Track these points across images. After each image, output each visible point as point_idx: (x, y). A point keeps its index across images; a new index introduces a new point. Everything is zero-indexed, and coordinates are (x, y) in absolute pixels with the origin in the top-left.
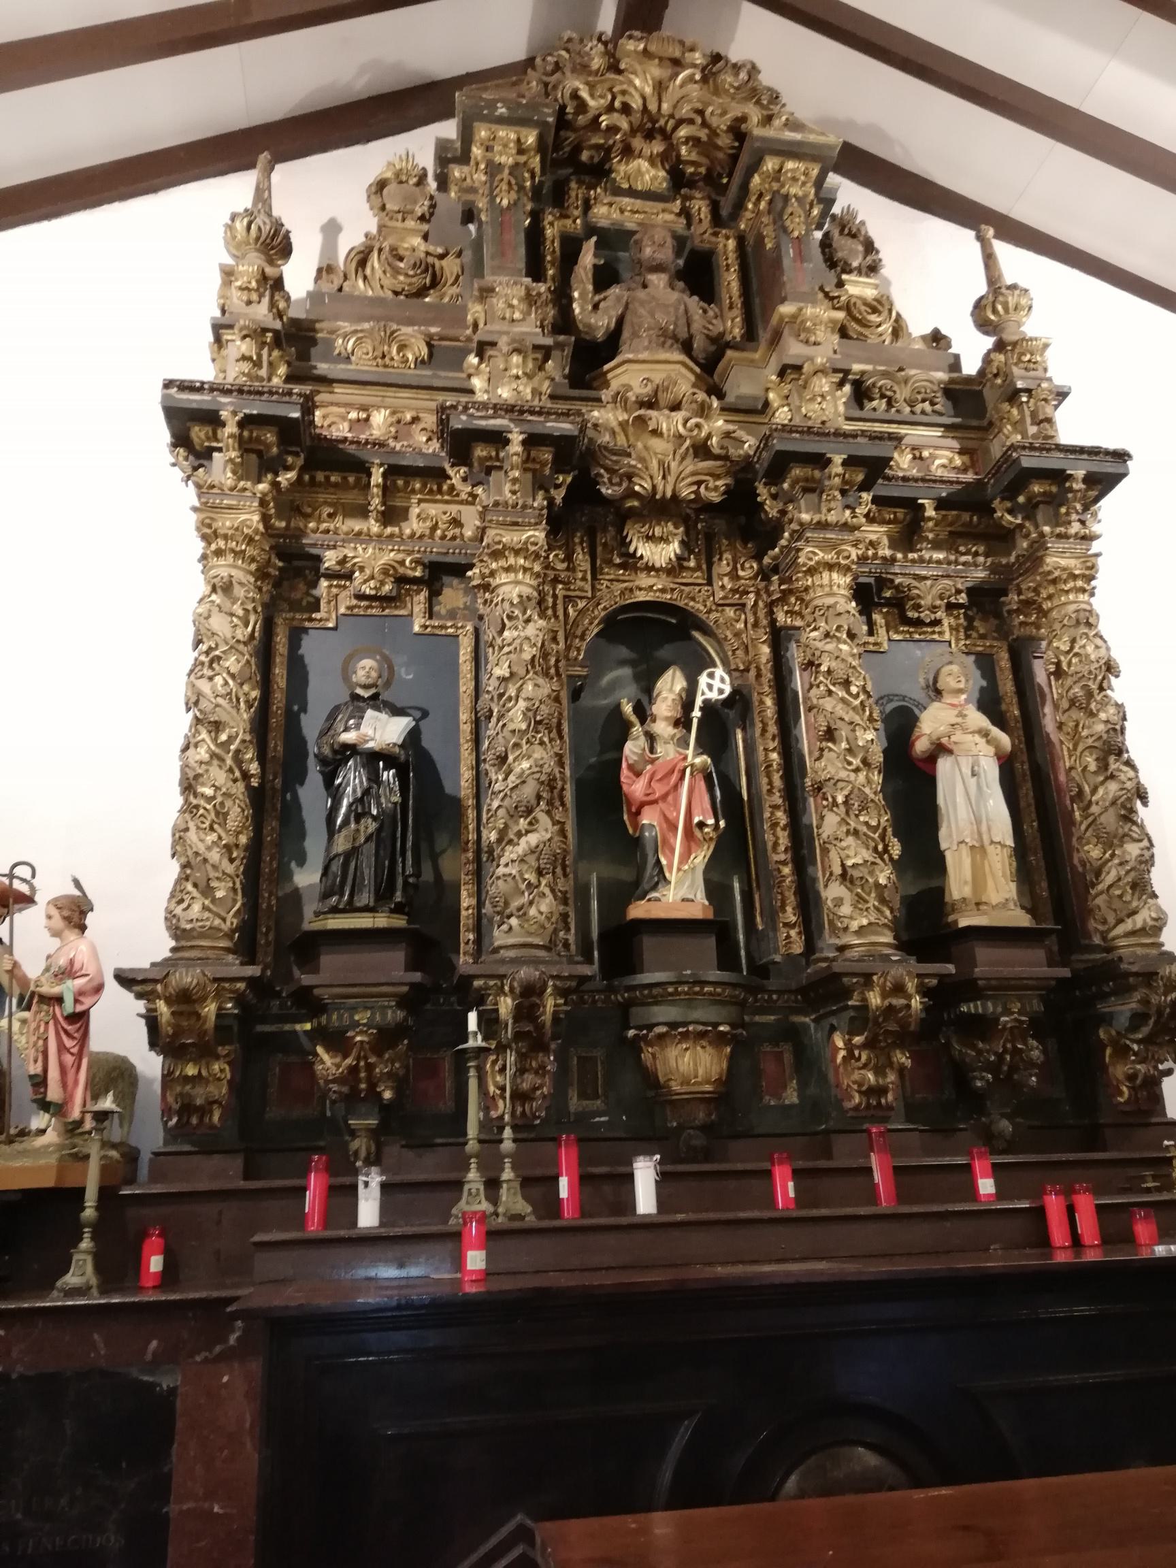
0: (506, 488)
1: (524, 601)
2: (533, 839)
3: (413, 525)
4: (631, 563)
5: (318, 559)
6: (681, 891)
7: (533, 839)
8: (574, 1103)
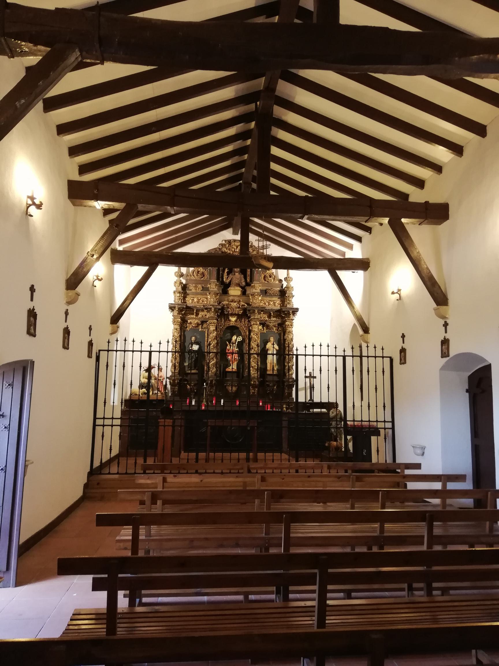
0: (212, 314)
1: (213, 330)
2: (213, 362)
3: (200, 316)
4: (230, 321)
5: (187, 321)
6: (233, 367)
7: (213, 362)
8: (218, 392)
